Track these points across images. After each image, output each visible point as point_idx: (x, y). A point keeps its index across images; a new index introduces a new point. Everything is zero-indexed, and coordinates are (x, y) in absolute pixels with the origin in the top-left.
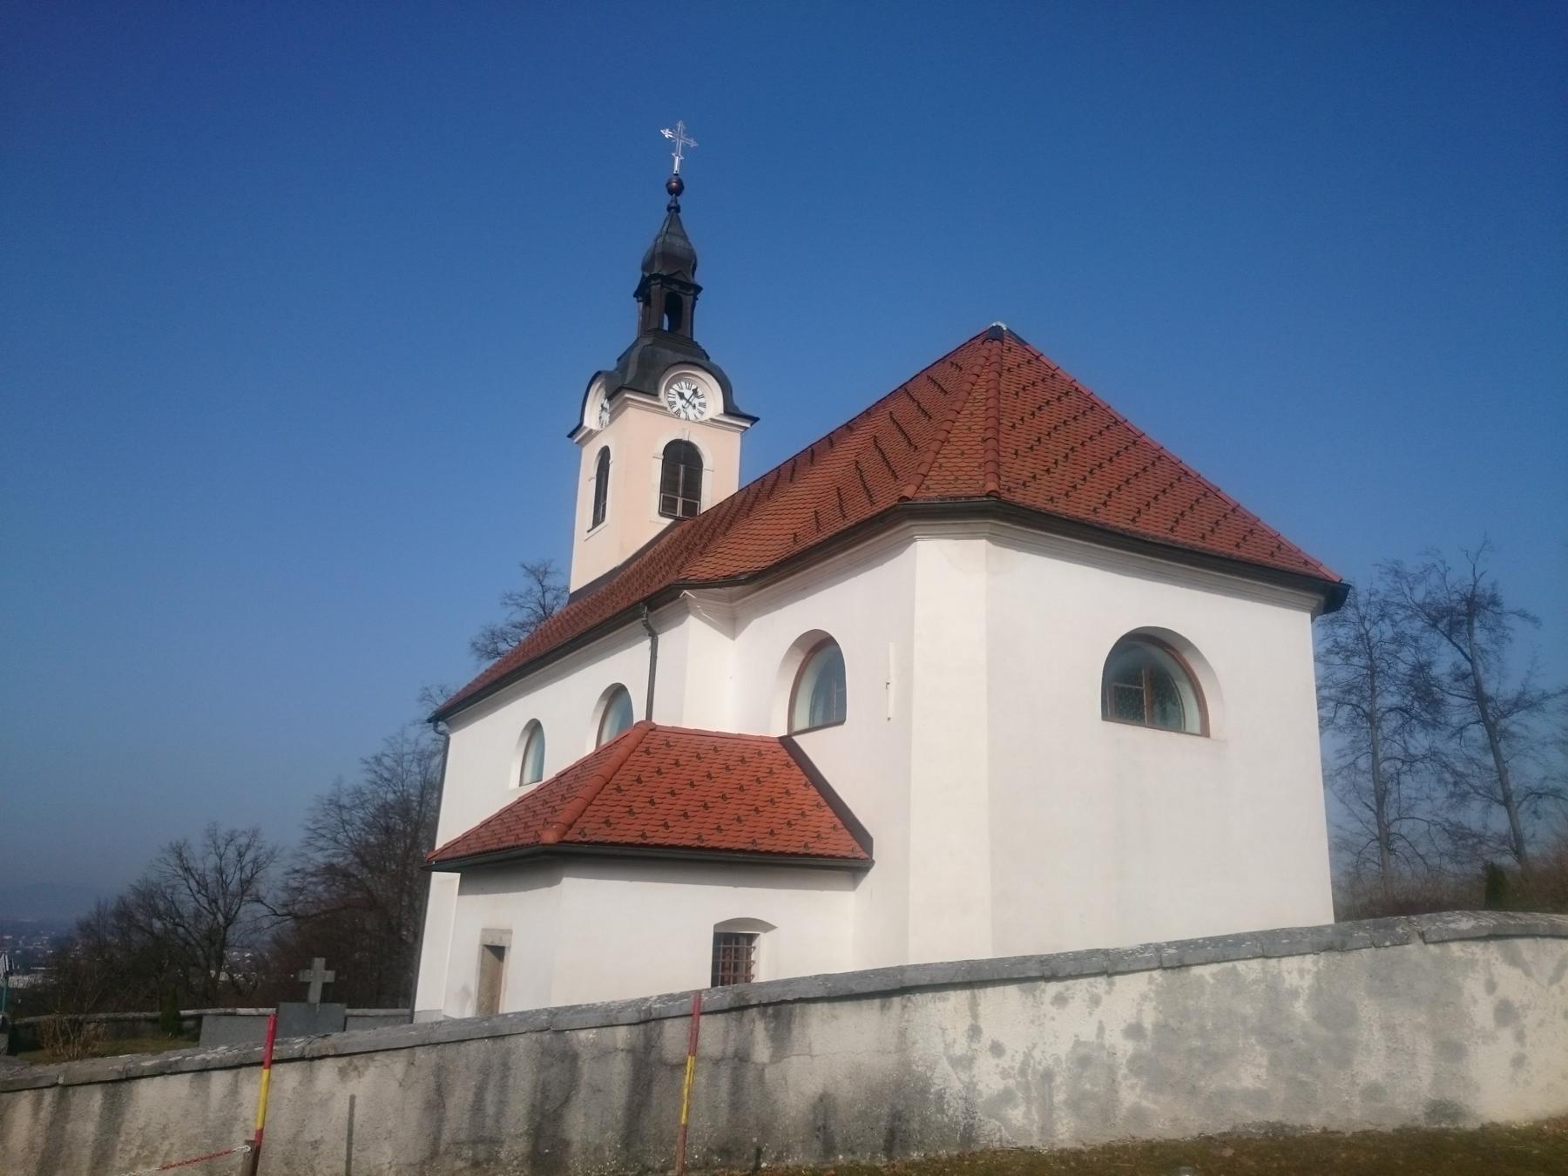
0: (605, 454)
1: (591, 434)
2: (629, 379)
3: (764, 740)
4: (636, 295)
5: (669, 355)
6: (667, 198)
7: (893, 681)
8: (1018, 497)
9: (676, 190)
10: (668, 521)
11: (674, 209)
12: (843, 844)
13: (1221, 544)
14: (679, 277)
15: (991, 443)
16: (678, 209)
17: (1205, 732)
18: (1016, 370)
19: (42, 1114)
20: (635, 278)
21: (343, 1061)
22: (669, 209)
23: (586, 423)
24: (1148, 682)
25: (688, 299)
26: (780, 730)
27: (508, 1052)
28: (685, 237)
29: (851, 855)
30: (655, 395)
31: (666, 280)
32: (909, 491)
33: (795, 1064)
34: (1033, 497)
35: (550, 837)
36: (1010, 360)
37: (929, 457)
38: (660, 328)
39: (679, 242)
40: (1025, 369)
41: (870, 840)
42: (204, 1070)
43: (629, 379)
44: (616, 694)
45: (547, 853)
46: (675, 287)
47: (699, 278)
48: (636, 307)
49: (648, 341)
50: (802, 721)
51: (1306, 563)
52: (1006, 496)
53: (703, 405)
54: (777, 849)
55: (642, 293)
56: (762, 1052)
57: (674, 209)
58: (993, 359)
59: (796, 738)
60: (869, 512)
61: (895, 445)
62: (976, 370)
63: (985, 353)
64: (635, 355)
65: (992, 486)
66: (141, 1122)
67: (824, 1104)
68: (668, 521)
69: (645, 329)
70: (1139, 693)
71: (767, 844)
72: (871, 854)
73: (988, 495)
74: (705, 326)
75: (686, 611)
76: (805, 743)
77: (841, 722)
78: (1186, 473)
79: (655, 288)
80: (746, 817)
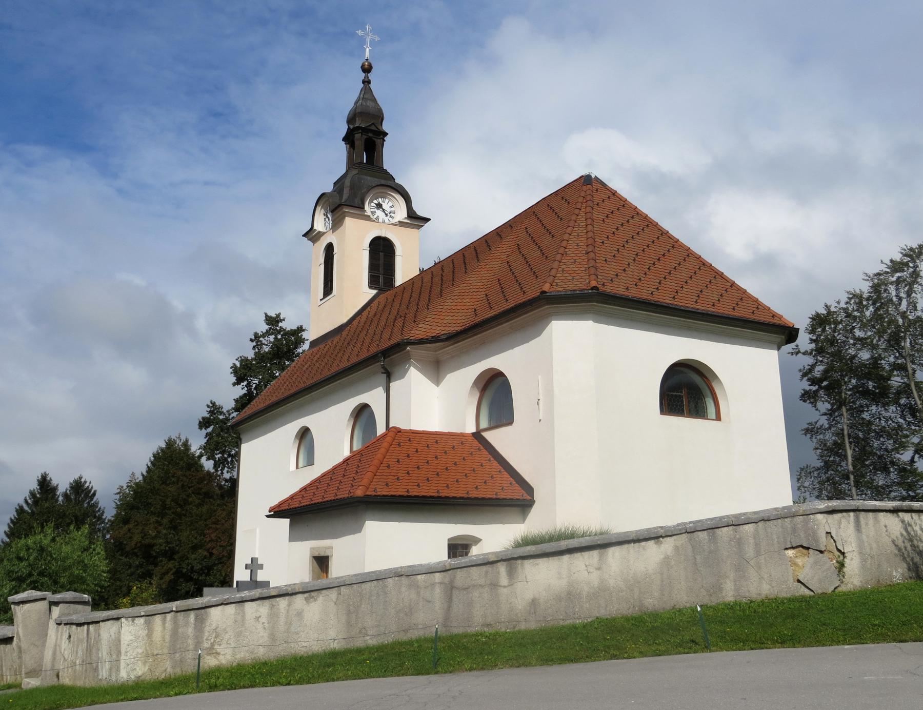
0: (329, 249)
1: (320, 235)
2: (345, 196)
3: (462, 435)
4: (343, 140)
5: (370, 180)
6: (362, 75)
7: (541, 397)
8: (609, 289)
9: (367, 69)
10: (374, 292)
11: (366, 82)
12: (518, 493)
13: (724, 309)
14: (373, 128)
15: (592, 255)
16: (369, 82)
17: (718, 418)
18: (601, 204)
19: (167, 625)
20: (343, 129)
21: (306, 595)
22: (364, 82)
23: (315, 227)
24: (686, 391)
25: (378, 141)
26: (471, 428)
27: (386, 586)
28: (375, 100)
29: (521, 498)
30: (362, 208)
31: (365, 130)
32: (546, 287)
33: (519, 586)
34: (618, 288)
35: (359, 493)
36: (597, 199)
37: (556, 264)
38: (362, 162)
39: (370, 104)
40: (607, 203)
41: (532, 489)
42: (243, 601)
43: (345, 196)
44: (362, 413)
45: (359, 502)
46: (370, 135)
47: (385, 127)
48: (343, 148)
49: (355, 172)
50: (484, 424)
51: (773, 316)
52: (601, 288)
53: (394, 212)
54: (481, 496)
55: (349, 139)
56: (504, 580)
57: (366, 82)
58: (589, 198)
59: (484, 434)
60: (523, 299)
61: (533, 253)
62: (579, 205)
63: (583, 194)
64: (347, 182)
65: (594, 283)
66: (214, 626)
67: (534, 602)
68: (374, 292)
69: (351, 163)
70: (681, 397)
71: (474, 494)
72: (532, 496)
73: (592, 289)
74: (391, 160)
75: (407, 359)
76: (489, 436)
77: (510, 422)
78: (704, 264)
79: (357, 136)
80: (452, 482)
